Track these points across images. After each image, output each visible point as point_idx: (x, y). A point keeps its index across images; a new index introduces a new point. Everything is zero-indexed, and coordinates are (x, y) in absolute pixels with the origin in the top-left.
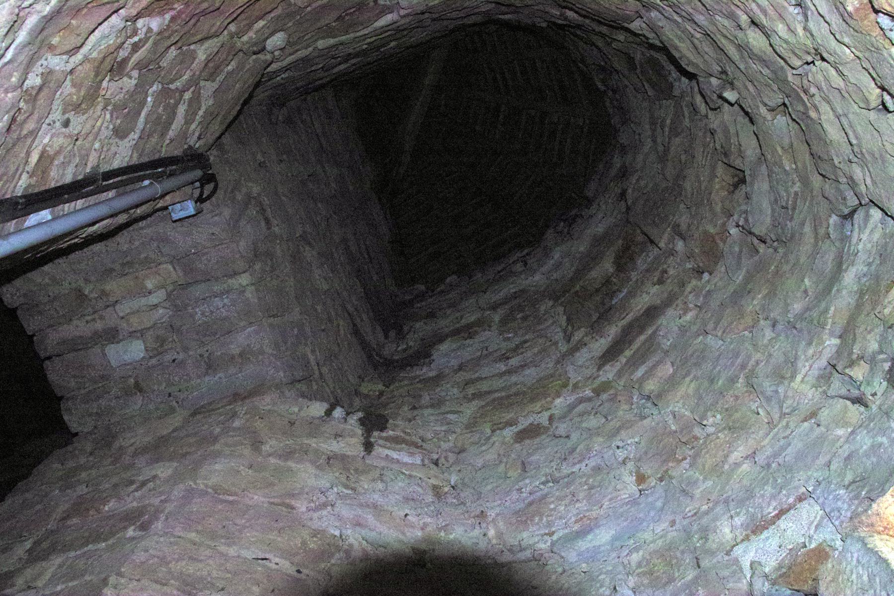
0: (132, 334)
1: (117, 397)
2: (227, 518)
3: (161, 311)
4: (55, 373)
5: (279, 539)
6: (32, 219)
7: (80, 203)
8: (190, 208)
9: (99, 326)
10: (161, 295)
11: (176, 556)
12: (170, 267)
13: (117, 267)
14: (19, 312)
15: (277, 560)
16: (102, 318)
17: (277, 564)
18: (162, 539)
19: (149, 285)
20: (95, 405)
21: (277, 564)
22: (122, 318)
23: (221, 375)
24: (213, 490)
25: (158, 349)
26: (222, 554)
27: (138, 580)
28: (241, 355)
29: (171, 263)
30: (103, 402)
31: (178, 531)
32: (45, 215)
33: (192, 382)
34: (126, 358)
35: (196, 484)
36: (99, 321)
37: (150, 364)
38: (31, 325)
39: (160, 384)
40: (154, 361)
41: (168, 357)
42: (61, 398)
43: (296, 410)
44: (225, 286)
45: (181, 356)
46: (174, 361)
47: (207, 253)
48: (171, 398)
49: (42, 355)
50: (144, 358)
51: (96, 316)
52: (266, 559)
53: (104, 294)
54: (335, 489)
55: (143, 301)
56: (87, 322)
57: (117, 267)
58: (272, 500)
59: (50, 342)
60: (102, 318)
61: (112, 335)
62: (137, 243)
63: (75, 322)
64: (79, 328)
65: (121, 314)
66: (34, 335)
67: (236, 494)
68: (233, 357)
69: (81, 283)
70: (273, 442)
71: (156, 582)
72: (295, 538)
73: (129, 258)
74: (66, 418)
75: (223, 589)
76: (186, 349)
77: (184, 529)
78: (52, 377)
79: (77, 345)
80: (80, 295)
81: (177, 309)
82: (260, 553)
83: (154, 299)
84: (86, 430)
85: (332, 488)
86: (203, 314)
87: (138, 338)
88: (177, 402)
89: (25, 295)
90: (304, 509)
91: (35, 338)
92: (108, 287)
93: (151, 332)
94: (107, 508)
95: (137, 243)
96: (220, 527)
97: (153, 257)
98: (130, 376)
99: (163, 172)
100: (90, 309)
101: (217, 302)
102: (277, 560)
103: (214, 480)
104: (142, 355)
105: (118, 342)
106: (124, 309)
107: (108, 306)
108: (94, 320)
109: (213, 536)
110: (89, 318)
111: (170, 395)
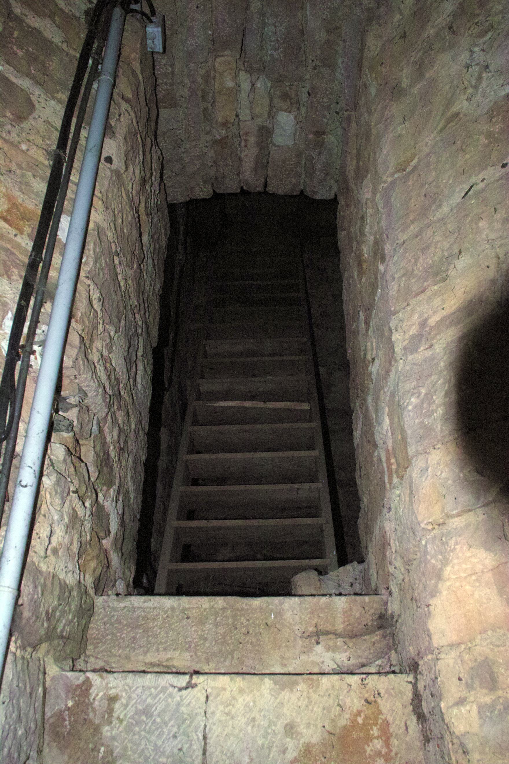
0: (272, 115)
1: (320, 153)
2: (422, 185)
3: (259, 86)
4: (280, 186)
5: (467, 156)
6: (62, 235)
7: (74, 177)
8: (153, 31)
9: (252, 139)
10: (243, 76)
11: (413, 261)
12: (219, 60)
13: (203, 105)
14: (218, 191)
15: (481, 176)
16: (247, 134)
17: (483, 180)
18: (396, 258)
19: (230, 84)
20: (318, 173)
21: (483, 180)
22: (253, 118)
23: (340, 60)
24: (398, 171)
25: (291, 101)
26: (73, 726)
27: (408, 305)
28: (329, 32)
29: (217, 56)
30: (319, 166)
31: (403, 237)
32: (64, 222)
33: (335, 88)
34: (289, 132)
35: (385, 182)
36: (248, 138)
37: (304, 114)
38: (231, 186)
39: (324, 116)
40: (303, 110)
41: (304, 97)
42: (302, 192)
43: (398, 17)
44: (255, 15)
45: (308, 86)
46: (309, 94)
47: (216, 21)
48: (341, 113)
49: (260, 189)
50: (295, 118)
51: (243, 138)
52: (471, 187)
53: (225, 124)
54: (476, 49)
55: (244, 95)
56: (246, 146)
57: (203, 105)
58: (439, 128)
59: (250, 178)
60: (247, 134)
61: (265, 133)
62: (187, 81)
63: (243, 155)
64: (249, 154)
65: (249, 118)
66: (242, 188)
67: (414, 155)
68: (328, 42)
69: (208, 138)
70: (405, 73)
71: (417, 294)
72: (478, 140)
73: (199, 93)
74: (318, 197)
75: (460, 252)
76: (301, 79)
77: (403, 231)
78: (281, 191)
79: (262, 162)
80: (222, 143)
81: (262, 70)
82: (464, 185)
83: (246, 86)
84: (336, 189)
85: (472, 52)
86: (276, 49)
87: (277, 113)
88: (346, 111)
89: (205, 182)
90: (465, 104)
91: (245, 188)
92: (220, 119)
93: (275, 100)
94: (366, 255)
95: (187, 81)
96: (423, 198)
97: (204, 71)
98: (307, 135)
99: (94, 59)
100: (236, 140)
101: (269, 31)
102: (481, 176)
103: (392, 162)
104: (292, 117)
105: (273, 130)
106: (245, 114)
107: (239, 125)
108: (246, 141)
109: (424, 211)
110: (243, 144)
111: (338, 113)
